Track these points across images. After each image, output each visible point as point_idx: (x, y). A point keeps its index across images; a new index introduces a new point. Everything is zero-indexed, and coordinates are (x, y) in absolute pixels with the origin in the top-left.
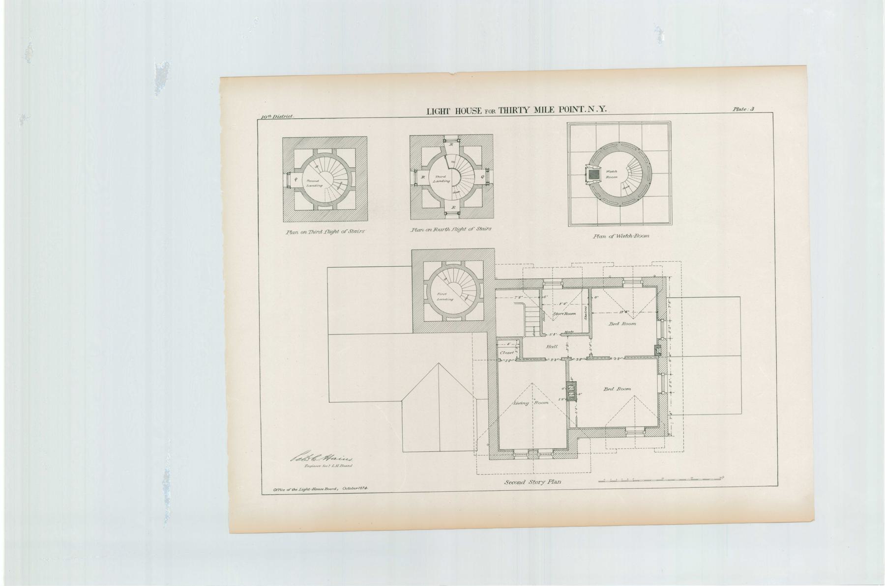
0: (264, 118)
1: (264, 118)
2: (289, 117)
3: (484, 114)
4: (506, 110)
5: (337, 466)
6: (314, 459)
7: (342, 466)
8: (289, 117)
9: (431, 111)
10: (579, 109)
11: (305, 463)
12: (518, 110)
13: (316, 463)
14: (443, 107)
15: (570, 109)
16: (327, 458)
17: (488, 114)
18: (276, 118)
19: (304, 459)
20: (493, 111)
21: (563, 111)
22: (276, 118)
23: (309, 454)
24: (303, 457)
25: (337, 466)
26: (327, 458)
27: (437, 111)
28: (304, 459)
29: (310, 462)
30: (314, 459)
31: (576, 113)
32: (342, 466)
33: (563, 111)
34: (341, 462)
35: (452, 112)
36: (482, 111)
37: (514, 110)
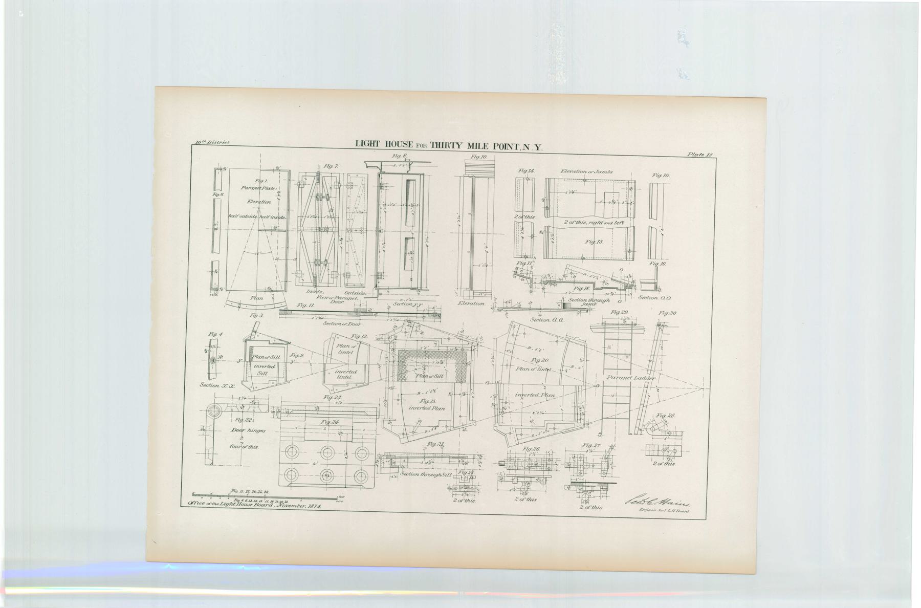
0: (198, 143)
1: (198, 143)
2: (224, 144)
3: (415, 148)
4: (438, 145)
5: (673, 511)
6: (649, 503)
7: (678, 511)
8: (224, 144)
9: (359, 143)
10: (514, 147)
11: (640, 506)
12: (451, 145)
13: (651, 507)
14: (373, 140)
15: (505, 147)
16: (663, 502)
17: (419, 148)
18: (210, 143)
19: (640, 503)
20: (423, 146)
21: (497, 148)
22: (210, 143)
23: (645, 497)
24: (638, 500)
25: (673, 511)
26: (663, 502)
27: (367, 143)
28: (640, 503)
29: (645, 506)
30: (649, 503)
31: (510, 150)
32: (678, 511)
33: (497, 148)
34: (678, 507)
35: (382, 145)
36: (414, 145)
37: (446, 145)
